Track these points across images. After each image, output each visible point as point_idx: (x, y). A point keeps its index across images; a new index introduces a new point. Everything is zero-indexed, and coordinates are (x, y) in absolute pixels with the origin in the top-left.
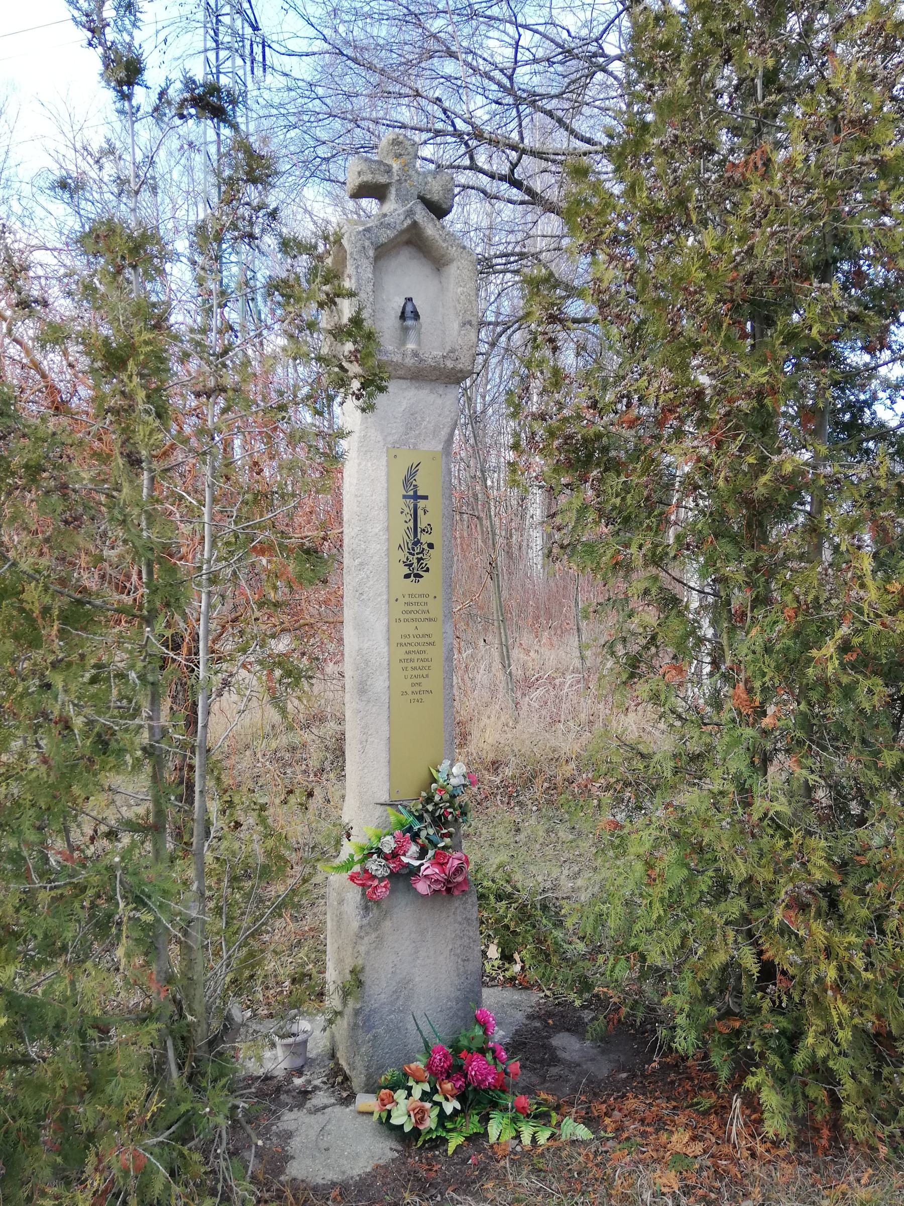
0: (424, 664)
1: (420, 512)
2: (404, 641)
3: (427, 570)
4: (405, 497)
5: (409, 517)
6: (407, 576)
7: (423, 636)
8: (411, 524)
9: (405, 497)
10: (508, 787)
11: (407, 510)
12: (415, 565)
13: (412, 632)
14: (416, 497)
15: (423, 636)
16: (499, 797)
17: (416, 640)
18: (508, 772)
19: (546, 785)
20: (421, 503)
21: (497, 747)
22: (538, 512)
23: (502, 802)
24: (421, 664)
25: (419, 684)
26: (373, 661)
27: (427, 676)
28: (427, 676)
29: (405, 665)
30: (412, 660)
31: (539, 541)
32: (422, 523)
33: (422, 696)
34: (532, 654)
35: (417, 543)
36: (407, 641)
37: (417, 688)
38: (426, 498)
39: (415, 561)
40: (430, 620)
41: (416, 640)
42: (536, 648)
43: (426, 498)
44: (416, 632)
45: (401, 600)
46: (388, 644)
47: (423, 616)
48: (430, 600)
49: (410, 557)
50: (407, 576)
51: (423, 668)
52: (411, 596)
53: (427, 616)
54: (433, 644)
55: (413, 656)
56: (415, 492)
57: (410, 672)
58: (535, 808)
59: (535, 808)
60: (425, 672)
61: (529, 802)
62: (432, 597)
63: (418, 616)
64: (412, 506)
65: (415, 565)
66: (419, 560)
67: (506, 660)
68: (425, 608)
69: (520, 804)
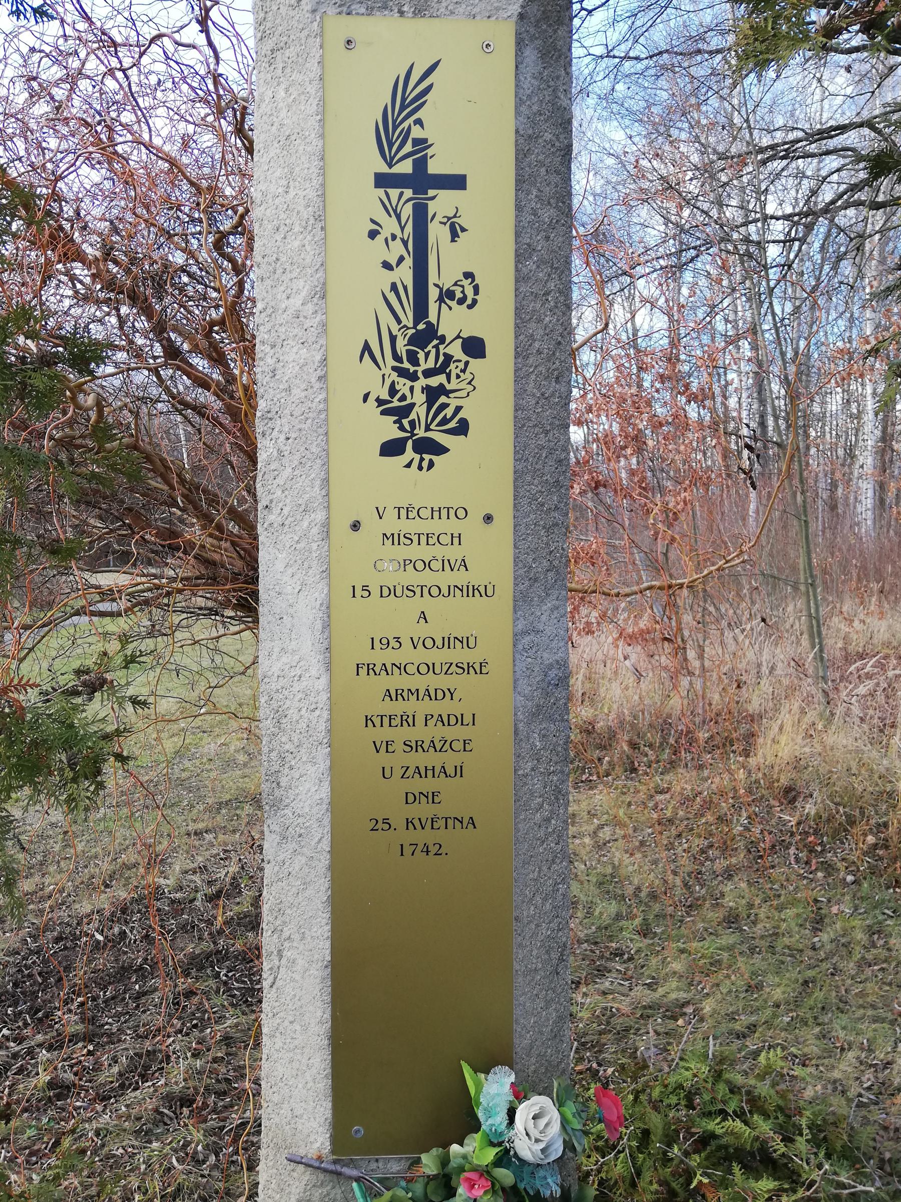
0: (449, 733)
1: (437, 232)
2: (380, 657)
3: (462, 428)
4: (382, 181)
5: (397, 248)
6: (391, 449)
7: (447, 643)
8: (405, 274)
9: (382, 181)
10: (807, 834)
11: (390, 226)
12: (420, 411)
13: (410, 629)
14: (422, 181)
15: (447, 643)
16: (792, 850)
17: (421, 656)
18: (810, 808)
19: (871, 839)
20: (442, 202)
21: (797, 764)
22: (870, 461)
23: (797, 860)
24: (438, 732)
25: (432, 797)
26: (293, 714)
27: (459, 771)
28: (459, 771)
29: (384, 733)
30: (407, 720)
31: (870, 493)
32: (445, 271)
33: (441, 835)
34: (856, 623)
35: (427, 336)
36: (389, 657)
37: (424, 810)
38: (457, 182)
39: (420, 398)
40: (472, 591)
41: (421, 656)
42: (862, 617)
43: (457, 182)
44: (422, 631)
45: (373, 528)
46: (329, 666)
47: (446, 579)
48: (471, 527)
49: (403, 386)
50: (391, 449)
51: (446, 745)
52: (406, 511)
53: (460, 578)
54: (481, 669)
55: (410, 706)
56: (421, 164)
57: (400, 759)
58: (850, 878)
59: (850, 878)
60: (450, 760)
61: (841, 865)
62: (476, 516)
63: (427, 578)
64: (407, 211)
65: (420, 411)
66: (433, 394)
67: (816, 632)
68: (454, 553)
69: (828, 868)
